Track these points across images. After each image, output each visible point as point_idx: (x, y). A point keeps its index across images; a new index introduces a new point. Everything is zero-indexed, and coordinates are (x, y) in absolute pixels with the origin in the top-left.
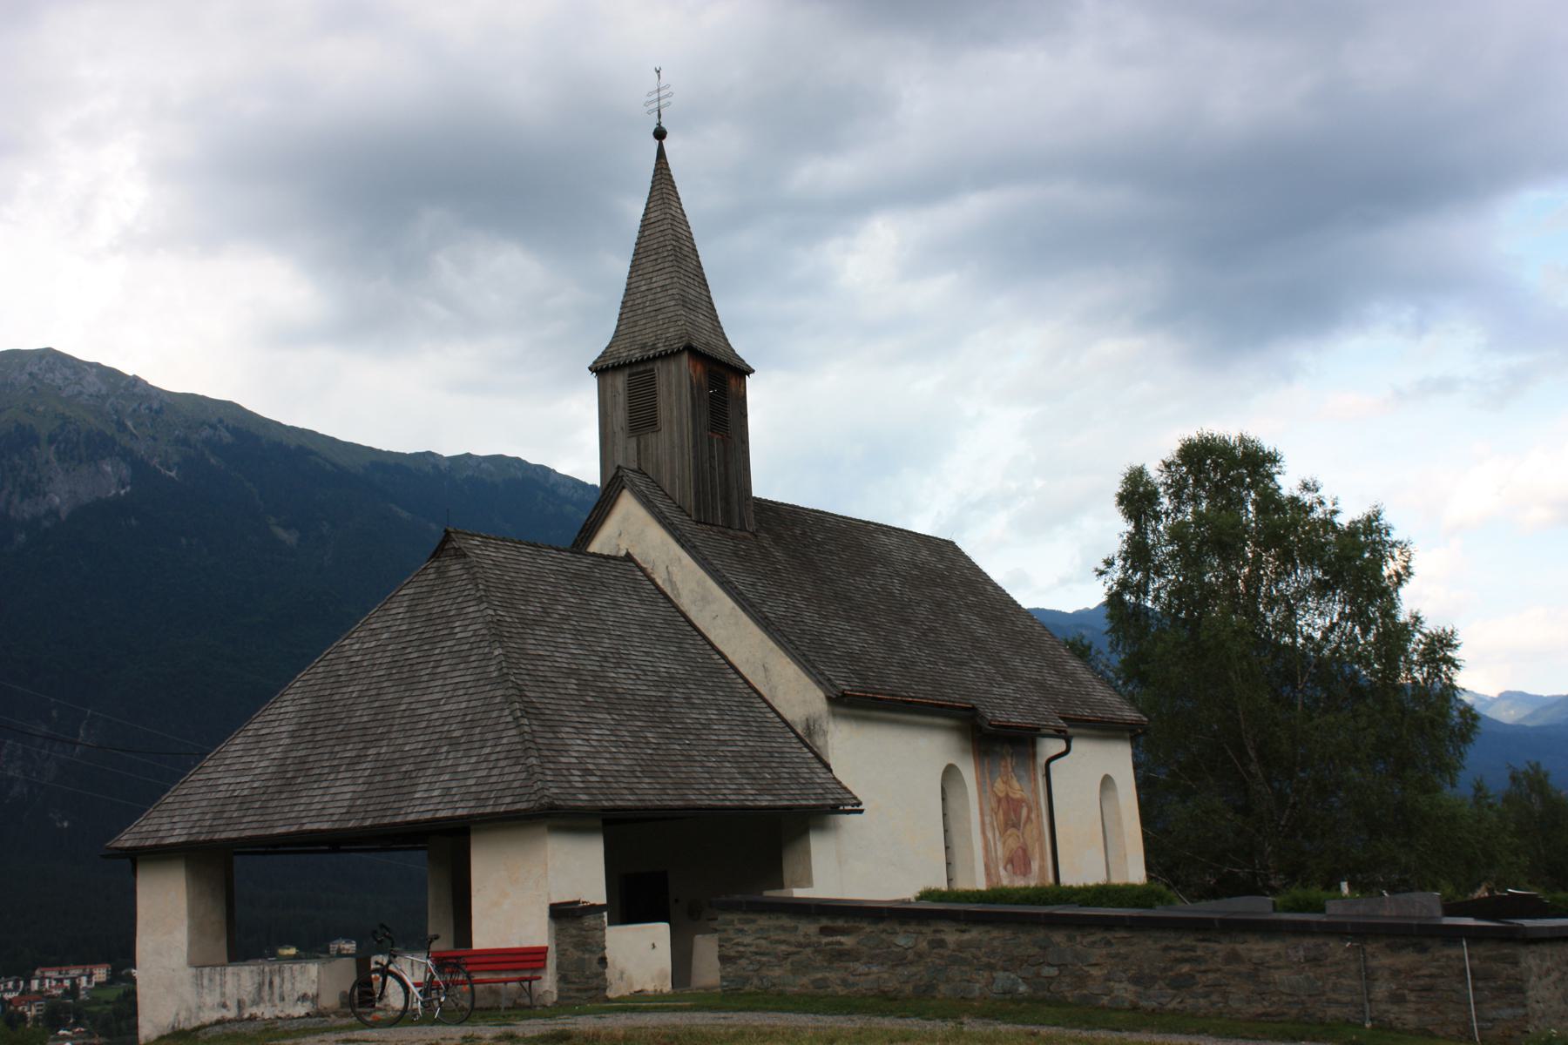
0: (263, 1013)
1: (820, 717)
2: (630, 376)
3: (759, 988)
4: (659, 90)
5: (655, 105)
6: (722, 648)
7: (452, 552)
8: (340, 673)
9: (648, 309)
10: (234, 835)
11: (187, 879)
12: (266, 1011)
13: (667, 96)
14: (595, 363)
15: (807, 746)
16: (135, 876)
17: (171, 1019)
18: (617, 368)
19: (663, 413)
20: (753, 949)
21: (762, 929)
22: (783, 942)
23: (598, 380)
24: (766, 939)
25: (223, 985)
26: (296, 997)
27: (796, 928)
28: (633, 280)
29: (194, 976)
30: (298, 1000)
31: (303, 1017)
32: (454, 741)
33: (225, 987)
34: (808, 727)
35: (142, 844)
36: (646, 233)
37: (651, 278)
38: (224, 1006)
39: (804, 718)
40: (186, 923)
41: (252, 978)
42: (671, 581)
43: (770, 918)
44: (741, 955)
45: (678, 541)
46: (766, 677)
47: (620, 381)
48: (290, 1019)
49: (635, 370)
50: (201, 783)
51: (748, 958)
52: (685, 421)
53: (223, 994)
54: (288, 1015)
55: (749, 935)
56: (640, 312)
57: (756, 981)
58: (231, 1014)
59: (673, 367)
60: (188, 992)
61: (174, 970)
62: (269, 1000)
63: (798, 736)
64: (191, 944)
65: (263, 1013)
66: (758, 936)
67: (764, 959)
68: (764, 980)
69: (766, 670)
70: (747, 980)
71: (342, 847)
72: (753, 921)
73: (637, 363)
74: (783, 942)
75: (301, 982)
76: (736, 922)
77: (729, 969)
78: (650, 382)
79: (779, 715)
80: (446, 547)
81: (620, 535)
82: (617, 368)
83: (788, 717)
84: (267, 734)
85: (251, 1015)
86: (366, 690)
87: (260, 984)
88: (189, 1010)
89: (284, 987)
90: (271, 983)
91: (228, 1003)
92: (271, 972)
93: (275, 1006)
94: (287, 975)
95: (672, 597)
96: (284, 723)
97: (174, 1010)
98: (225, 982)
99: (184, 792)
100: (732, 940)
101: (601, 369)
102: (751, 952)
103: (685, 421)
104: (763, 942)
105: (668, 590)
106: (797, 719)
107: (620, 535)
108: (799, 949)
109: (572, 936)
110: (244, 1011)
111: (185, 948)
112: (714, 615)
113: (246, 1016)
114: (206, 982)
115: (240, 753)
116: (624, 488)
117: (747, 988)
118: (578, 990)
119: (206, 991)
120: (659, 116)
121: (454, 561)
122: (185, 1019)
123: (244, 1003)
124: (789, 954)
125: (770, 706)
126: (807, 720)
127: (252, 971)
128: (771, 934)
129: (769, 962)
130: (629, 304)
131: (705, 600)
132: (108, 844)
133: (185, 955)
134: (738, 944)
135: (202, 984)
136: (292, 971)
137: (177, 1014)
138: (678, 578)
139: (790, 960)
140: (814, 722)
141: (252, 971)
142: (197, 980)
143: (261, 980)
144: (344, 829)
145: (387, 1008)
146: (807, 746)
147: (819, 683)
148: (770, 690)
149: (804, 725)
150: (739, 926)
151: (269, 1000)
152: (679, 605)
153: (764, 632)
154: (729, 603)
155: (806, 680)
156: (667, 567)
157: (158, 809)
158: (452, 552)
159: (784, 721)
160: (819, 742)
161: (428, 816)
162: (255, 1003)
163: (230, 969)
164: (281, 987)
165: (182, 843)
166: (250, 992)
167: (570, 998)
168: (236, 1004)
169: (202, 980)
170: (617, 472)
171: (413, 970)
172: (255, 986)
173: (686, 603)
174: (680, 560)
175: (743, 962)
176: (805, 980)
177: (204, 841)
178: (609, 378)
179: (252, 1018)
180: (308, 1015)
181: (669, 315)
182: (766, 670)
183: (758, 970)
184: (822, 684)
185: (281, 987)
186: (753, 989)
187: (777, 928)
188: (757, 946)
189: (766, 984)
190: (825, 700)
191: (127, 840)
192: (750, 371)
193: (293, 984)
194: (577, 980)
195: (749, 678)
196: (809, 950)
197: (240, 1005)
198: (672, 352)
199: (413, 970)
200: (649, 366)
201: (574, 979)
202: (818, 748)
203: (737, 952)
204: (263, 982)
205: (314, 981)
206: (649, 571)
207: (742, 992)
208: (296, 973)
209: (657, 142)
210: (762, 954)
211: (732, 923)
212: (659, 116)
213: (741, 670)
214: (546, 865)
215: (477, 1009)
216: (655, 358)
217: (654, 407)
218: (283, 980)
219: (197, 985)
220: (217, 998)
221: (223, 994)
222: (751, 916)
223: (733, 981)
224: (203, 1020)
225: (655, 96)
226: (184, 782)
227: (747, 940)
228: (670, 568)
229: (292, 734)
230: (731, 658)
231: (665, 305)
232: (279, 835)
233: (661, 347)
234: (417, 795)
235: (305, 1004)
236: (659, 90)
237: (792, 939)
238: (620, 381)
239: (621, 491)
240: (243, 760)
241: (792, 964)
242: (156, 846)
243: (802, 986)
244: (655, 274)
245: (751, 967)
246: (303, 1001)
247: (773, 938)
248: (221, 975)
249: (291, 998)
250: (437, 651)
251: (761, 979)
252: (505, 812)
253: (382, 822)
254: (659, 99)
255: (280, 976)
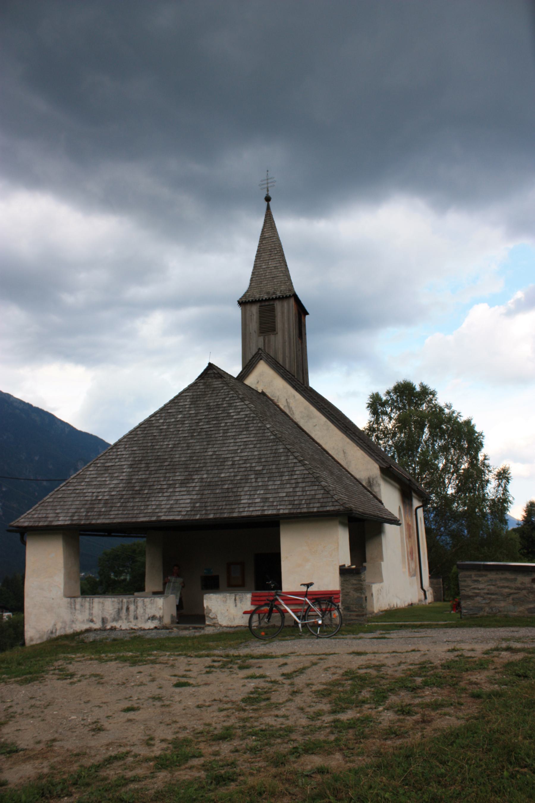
0: (121, 626)
1: (376, 477)
2: (260, 306)
3: (490, 613)
4: (267, 179)
5: (266, 186)
6: (318, 441)
7: (212, 375)
8: (155, 434)
9: (268, 277)
10: (107, 521)
11: (63, 548)
12: (123, 625)
13: (263, 184)
14: (240, 299)
15: (369, 491)
16: (24, 543)
17: (50, 627)
18: (253, 302)
19: (279, 325)
20: (486, 591)
21: (491, 580)
22: (507, 587)
23: (242, 309)
24: (493, 585)
25: (91, 608)
26: (147, 617)
27: (515, 580)
28: (258, 263)
29: (68, 603)
30: (149, 619)
31: (152, 629)
32: (258, 472)
33: (92, 610)
34: (369, 482)
35: (36, 525)
36: (264, 242)
37: (268, 263)
38: (92, 621)
39: (367, 477)
40: (62, 571)
41: (113, 605)
42: (289, 407)
43: (497, 574)
44: (477, 595)
45: (294, 387)
46: (345, 456)
47: (254, 309)
48: (141, 630)
49: (263, 304)
50: (71, 492)
51: (481, 597)
52: (292, 330)
53: (91, 614)
54: (141, 628)
55: (482, 583)
56: (263, 277)
57: (487, 609)
58: (97, 625)
59: (285, 304)
60: (65, 614)
61: (53, 599)
62: (126, 619)
63: (363, 486)
64: (66, 583)
65: (121, 626)
66: (489, 584)
67: (493, 597)
68: (494, 609)
69: (344, 453)
70: (481, 609)
71: (113, 534)
72: (485, 576)
73: (266, 300)
74: (507, 587)
75: (151, 609)
76: (473, 576)
77: (469, 603)
78: (273, 310)
79: (352, 475)
80: (209, 372)
81: (258, 382)
82: (253, 302)
83: (358, 477)
84: (112, 466)
85: (112, 627)
86: (178, 444)
87: (119, 609)
88: (64, 622)
89: (138, 612)
90: (128, 609)
91: (94, 619)
92: (128, 602)
93: (131, 622)
94: (140, 604)
95: (289, 414)
96: (122, 460)
97: (53, 623)
98: (93, 607)
99: (60, 496)
100: (470, 586)
101: (243, 303)
102: (484, 593)
103: (292, 330)
104: (492, 587)
105: (287, 411)
106: (362, 478)
107: (258, 382)
108: (517, 591)
109: (353, 584)
110: (107, 624)
111: (62, 586)
112: (315, 424)
113: (108, 627)
114: (78, 606)
115: (95, 476)
116: (261, 359)
117: (481, 614)
118: (357, 616)
119: (77, 612)
120: (268, 191)
121: (215, 380)
122: (61, 628)
123: (107, 619)
124: (511, 594)
125: (347, 471)
126: (369, 478)
127: (113, 602)
128: (498, 582)
129: (497, 598)
130: (256, 273)
131: (310, 417)
132: (12, 523)
133: (62, 591)
134: (474, 588)
135: (75, 608)
136: (144, 602)
137: (55, 625)
138: (293, 405)
139: (511, 597)
140: (373, 479)
141: (113, 602)
142: (71, 605)
143: (120, 607)
144: (193, 520)
145: (216, 625)
146: (369, 491)
147: (376, 461)
148: (347, 463)
149: (367, 481)
150: (475, 578)
151: (126, 619)
152: (293, 419)
153: (344, 434)
154: (323, 419)
155: (367, 458)
156: (287, 400)
157: (42, 505)
158: (212, 375)
159: (355, 478)
160: (376, 489)
161: (259, 513)
162: (115, 620)
163: (79, 600)
164: (135, 611)
165: (68, 525)
166: (111, 614)
167: (352, 620)
168: (101, 620)
169: (75, 605)
170: (258, 351)
171: (236, 603)
172: (116, 610)
173: (298, 417)
174: (294, 396)
175: (478, 599)
176: (521, 609)
177: (84, 525)
178: (248, 307)
179: (113, 629)
180: (156, 628)
181: (280, 280)
182: (344, 453)
183: (489, 603)
184: (378, 460)
185: (135, 611)
186: (486, 614)
187: (501, 579)
188: (488, 590)
189: (494, 611)
190: (379, 469)
191: (23, 521)
192: (307, 314)
193: (145, 610)
194: (357, 610)
195: (334, 456)
196: (524, 592)
197: (104, 621)
198: (283, 297)
199: (236, 603)
200: (271, 303)
201: (355, 609)
202: (375, 492)
203: (474, 593)
204: (122, 608)
205: (160, 608)
206: (276, 400)
207: (478, 615)
208: (147, 604)
209: (266, 203)
210: (492, 594)
211: (470, 576)
212: (268, 191)
213: (330, 452)
214: (338, 543)
215: (286, 626)
216: (276, 299)
217: (274, 322)
218: (137, 607)
219: (71, 608)
220: (86, 616)
221: (91, 614)
222: (484, 573)
223: (471, 609)
224: (75, 629)
225: (266, 182)
226: (58, 490)
227: (481, 586)
228: (288, 400)
229: (131, 466)
230: (324, 446)
231: (278, 275)
232: (142, 522)
233: (279, 294)
234: (242, 502)
235: (153, 621)
236: (267, 179)
237: (513, 585)
238: (254, 309)
239: (259, 361)
240: (98, 479)
241: (513, 599)
242: (47, 526)
243: (520, 612)
244: (270, 261)
245: (484, 602)
246: (152, 620)
247: (499, 585)
248: (90, 603)
249: (143, 618)
250: (223, 425)
251: (491, 608)
252: (318, 512)
253: (194, 518)
254: (268, 183)
255: (134, 605)
